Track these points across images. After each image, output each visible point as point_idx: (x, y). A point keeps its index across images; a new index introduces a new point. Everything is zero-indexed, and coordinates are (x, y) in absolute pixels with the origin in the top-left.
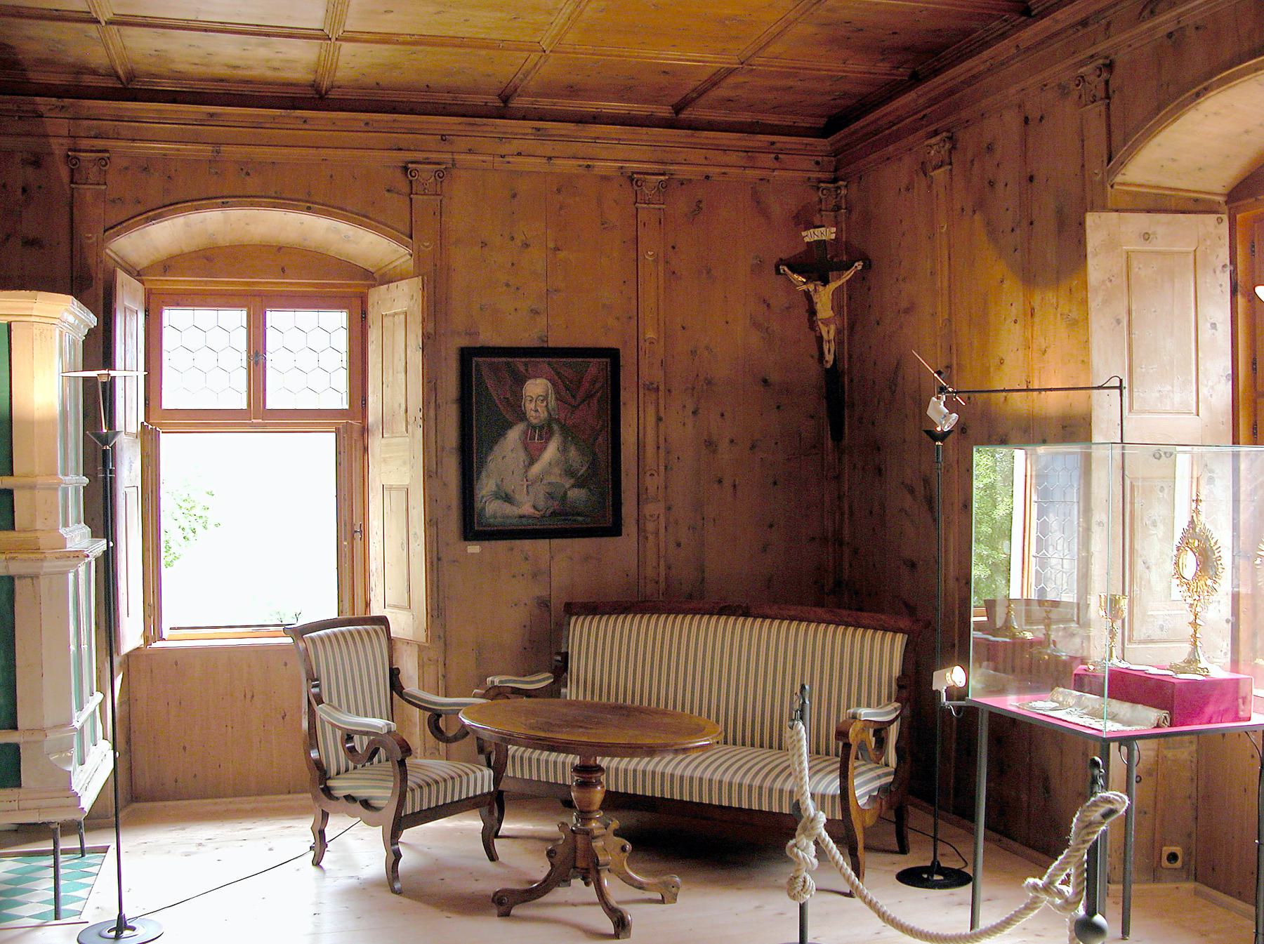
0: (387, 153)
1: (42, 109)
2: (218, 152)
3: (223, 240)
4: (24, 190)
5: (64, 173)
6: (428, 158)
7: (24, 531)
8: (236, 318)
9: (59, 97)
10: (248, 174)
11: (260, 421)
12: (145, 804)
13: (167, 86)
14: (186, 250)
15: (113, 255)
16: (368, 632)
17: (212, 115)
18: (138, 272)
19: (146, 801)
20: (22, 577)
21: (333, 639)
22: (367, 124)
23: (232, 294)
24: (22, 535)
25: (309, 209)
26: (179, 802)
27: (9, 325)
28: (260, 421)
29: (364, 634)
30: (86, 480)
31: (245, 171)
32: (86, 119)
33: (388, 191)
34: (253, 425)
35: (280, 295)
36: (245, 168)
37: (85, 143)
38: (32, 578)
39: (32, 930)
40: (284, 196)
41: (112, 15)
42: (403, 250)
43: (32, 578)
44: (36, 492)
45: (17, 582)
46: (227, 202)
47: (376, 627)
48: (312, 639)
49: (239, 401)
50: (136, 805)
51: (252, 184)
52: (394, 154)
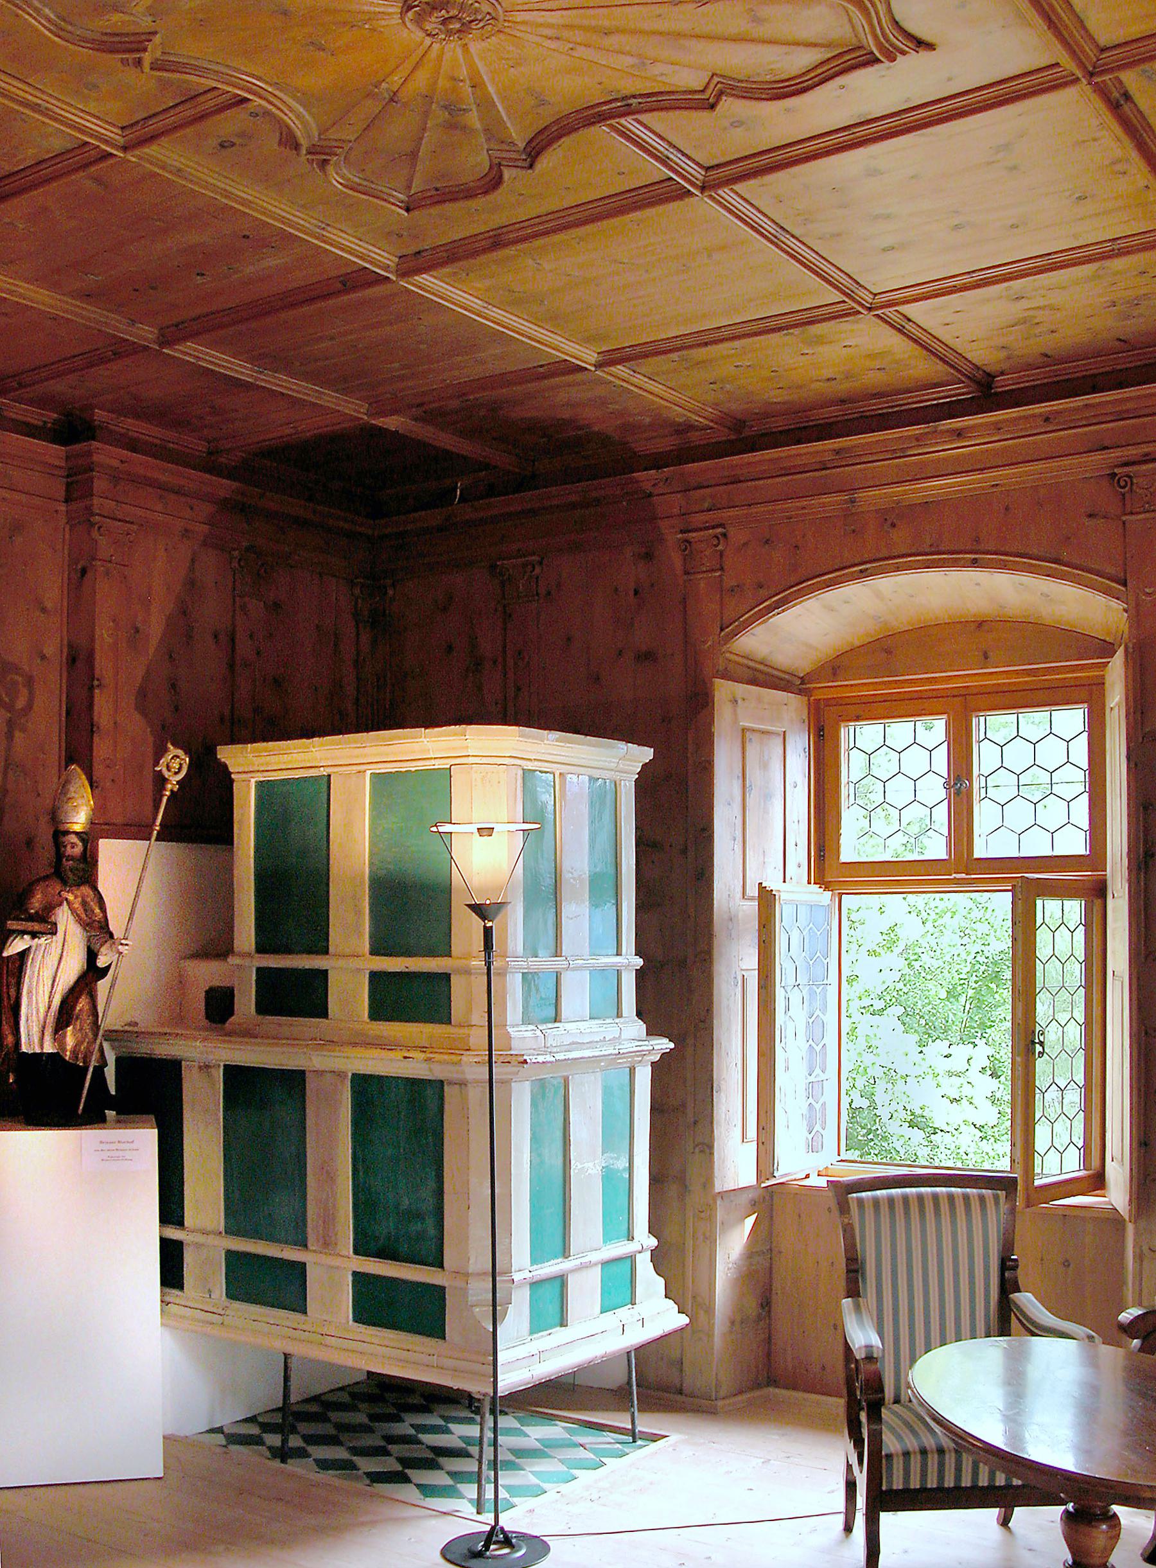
0: (1084, 459)
1: (647, 487)
2: (853, 501)
3: (901, 622)
4: (636, 592)
5: (678, 563)
6: (1147, 455)
7: (461, 1026)
8: (935, 730)
9: (658, 468)
10: (893, 525)
11: (963, 876)
12: (784, 1392)
13: (778, 424)
14: (857, 643)
15: (741, 660)
16: (982, 1198)
17: (837, 452)
18: (802, 678)
19: (786, 1387)
20: (450, 1083)
21: (899, 1208)
22: (1047, 420)
23: (1065, 686)
24: (457, 1030)
25: (974, 563)
26: (824, 1398)
27: (329, 776)
28: (963, 876)
29: (975, 1205)
30: (640, 962)
31: (889, 522)
32: (695, 489)
33: (1090, 516)
34: (958, 882)
35: (999, 691)
36: (891, 517)
37: (699, 519)
38: (461, 1084)
39: (436, 1516)
40: (943, 548)
41: (596, 355)
42: (1116, 605)
43: (461, 1084)
44: (473, 977)
45: (446, 1088)
46: (867, 569)
47: (987, 1192)
48: (860, 1202)
49: (936, 848)
50: (772, 1390)
51: (900, 537)
52: (1097, 457)
